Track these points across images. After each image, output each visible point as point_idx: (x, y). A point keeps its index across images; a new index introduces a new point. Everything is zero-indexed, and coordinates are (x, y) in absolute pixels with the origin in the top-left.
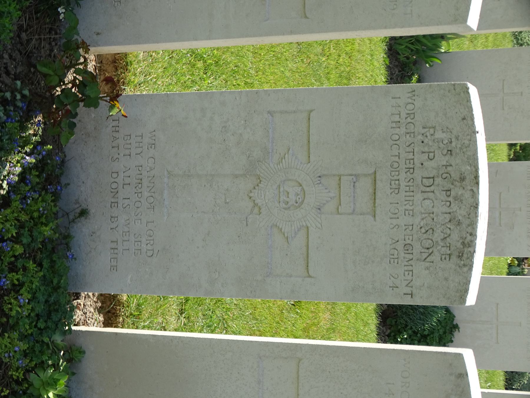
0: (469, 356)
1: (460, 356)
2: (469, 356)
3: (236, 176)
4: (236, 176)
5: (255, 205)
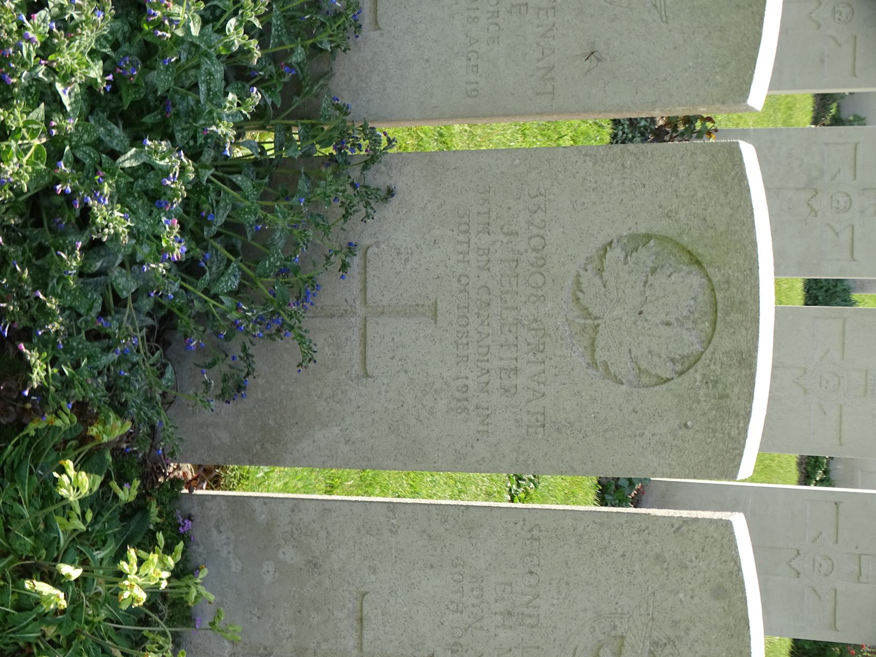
0: (739, 522)
1: (728, 524)
2: (739, 522)
3: (798, 189)
4: (798, 189)
5: (813, 210)
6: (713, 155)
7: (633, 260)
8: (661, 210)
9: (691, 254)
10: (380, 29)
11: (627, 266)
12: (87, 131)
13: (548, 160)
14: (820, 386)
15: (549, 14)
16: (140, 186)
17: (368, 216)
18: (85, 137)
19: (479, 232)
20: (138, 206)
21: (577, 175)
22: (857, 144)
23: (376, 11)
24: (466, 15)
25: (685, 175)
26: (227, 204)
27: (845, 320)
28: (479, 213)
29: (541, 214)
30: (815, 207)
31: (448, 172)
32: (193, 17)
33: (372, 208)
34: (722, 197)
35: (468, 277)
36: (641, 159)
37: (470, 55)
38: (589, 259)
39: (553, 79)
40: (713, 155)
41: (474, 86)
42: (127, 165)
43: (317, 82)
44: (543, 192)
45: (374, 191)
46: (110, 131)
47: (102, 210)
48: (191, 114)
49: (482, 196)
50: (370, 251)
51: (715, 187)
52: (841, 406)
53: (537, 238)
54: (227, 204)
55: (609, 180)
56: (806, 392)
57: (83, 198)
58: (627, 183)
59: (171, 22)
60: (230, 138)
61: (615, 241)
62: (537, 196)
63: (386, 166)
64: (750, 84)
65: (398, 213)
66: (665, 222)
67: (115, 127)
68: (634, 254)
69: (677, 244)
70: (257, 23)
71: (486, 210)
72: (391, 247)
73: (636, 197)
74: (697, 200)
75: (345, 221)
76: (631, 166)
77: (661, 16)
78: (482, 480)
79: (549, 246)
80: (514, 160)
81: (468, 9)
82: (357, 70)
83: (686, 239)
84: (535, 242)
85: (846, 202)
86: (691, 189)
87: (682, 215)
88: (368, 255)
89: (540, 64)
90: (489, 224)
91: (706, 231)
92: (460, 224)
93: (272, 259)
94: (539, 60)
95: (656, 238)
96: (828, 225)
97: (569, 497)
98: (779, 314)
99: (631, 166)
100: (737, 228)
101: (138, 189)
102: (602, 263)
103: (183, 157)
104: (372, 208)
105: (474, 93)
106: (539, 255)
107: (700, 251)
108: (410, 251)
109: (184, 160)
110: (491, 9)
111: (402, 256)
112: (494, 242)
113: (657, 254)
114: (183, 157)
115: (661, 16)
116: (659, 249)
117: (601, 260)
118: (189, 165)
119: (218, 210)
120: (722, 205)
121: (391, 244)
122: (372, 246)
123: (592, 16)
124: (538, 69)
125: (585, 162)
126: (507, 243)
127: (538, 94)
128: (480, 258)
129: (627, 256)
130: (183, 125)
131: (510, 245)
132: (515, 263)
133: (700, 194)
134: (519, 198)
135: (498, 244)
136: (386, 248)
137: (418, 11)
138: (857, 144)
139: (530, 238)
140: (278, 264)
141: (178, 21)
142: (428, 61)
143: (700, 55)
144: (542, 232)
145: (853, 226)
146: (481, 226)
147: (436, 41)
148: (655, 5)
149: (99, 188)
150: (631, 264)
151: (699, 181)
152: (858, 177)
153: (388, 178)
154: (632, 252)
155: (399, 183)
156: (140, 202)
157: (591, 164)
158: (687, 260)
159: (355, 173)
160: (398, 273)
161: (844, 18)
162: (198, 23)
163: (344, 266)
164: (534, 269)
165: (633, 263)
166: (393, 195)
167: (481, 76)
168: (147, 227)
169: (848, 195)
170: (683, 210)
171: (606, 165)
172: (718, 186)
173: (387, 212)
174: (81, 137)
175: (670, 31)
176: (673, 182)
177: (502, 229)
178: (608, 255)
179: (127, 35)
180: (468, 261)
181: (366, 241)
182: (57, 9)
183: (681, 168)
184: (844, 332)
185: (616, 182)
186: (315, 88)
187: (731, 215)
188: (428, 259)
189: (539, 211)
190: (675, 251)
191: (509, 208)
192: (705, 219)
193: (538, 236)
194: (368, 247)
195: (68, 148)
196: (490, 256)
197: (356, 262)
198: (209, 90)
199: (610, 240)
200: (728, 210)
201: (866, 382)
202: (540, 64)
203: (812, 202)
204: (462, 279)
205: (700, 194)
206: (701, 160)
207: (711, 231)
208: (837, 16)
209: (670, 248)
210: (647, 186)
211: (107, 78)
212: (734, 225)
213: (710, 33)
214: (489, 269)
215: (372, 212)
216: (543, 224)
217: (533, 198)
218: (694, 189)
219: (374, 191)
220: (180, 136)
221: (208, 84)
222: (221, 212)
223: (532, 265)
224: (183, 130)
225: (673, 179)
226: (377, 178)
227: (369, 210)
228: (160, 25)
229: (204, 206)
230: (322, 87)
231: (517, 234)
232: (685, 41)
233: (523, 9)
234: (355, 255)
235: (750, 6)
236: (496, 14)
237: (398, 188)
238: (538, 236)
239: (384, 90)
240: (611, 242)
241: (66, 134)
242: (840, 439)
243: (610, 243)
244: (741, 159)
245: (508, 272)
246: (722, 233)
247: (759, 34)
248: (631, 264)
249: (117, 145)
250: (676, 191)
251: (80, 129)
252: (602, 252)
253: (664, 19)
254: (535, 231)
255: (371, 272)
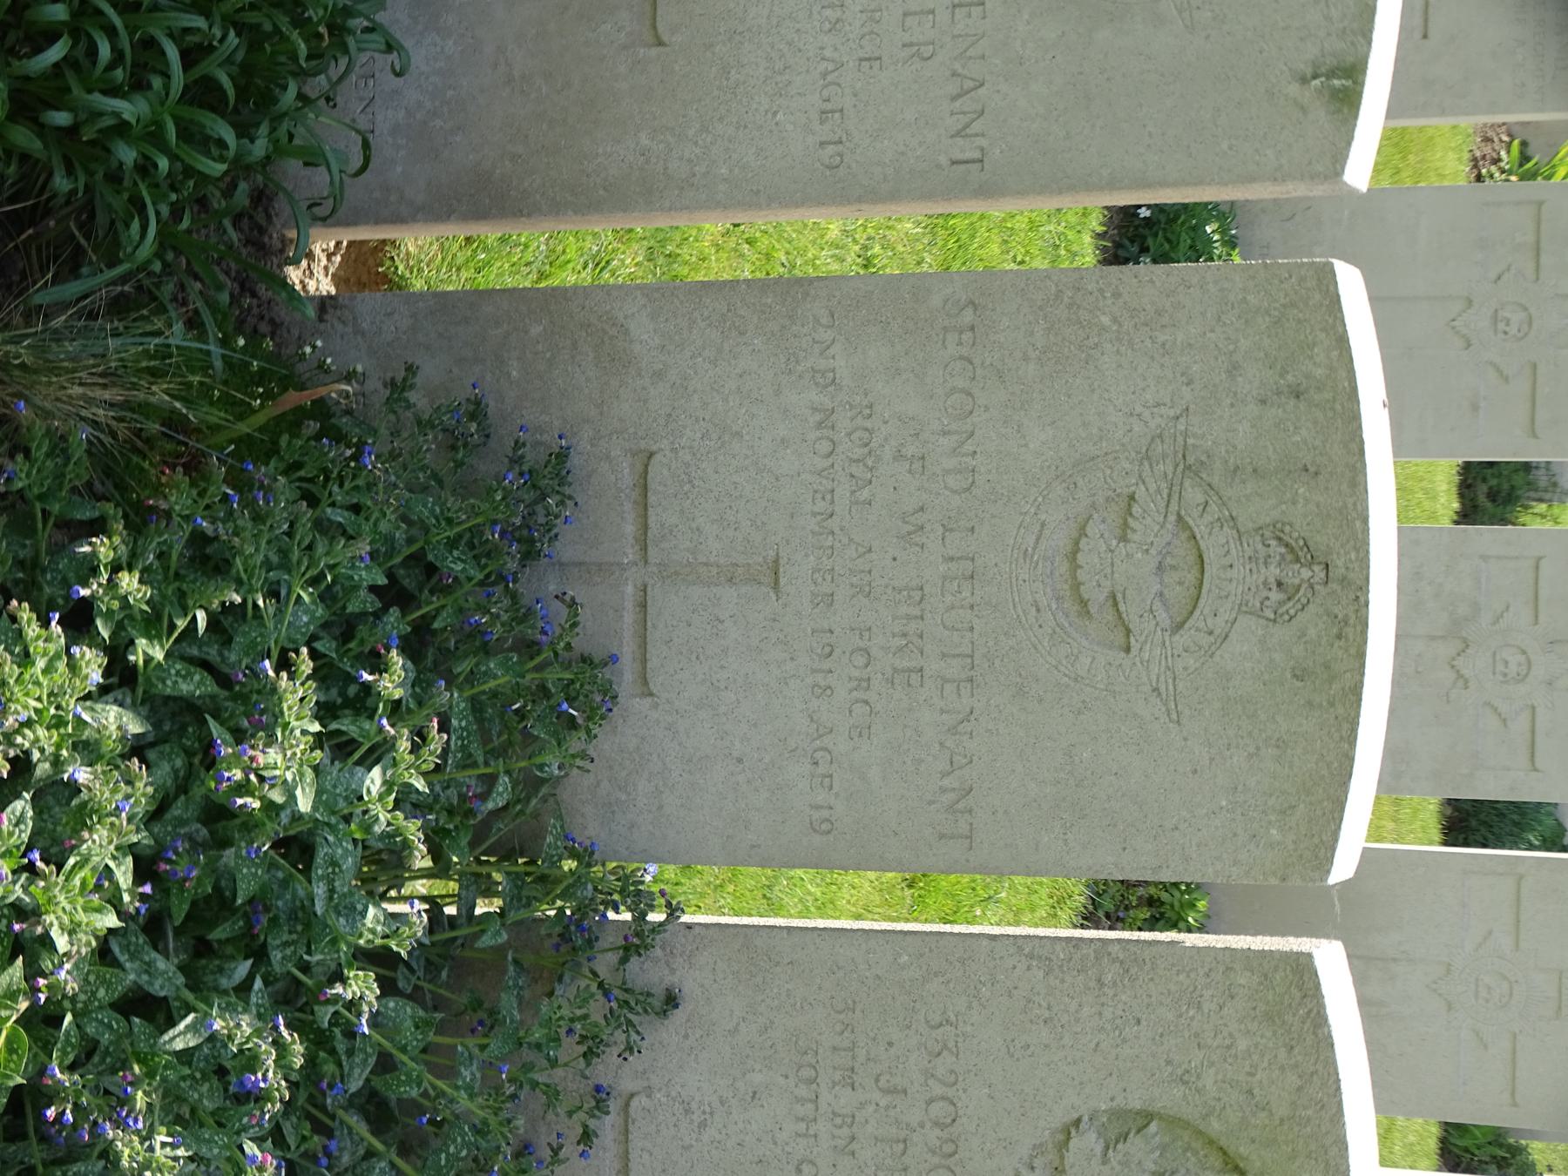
2: (1331, 962)
3: (1433, 638)
4: (1433, 638)
5: (1460, 676)
6: (1266, 976)
7: (1119, 1157)
8: (1170, 1069)
9: (1225, 1153)
10: (651, 694)
11: (1107, 1167)
12: (103, 982)
13: (962, 961)
14: (1477, 996)
15: (963, 691)
16: (206, 1059)
17: (630, 1049)
18: (101, 993)
19: (834, 1084)
20: (201, 1096)
21: (1015, 992)
22: (1539, 559)
23: (644, 661)
24: (809, 680)
25: (1214, 1007)
26: (368, 1055)
27: (1521, 877)
28: (835, 1048)
29: (947, 1058)
30: (1464, 671)
31: (778, 969)
32: (302, 775)
33: (638, 1033)
34: (1282, 1053)
35: (814, 1164)
36: (1133, 971)
37: (819, 755)
38: (1039, 1149)
39: (970, 811)
40: (1266, 976)
41: (825, 813)
42: (179, 1045)
43: (537, 791)
44: (953, 1018)
45: (641, 998)
46: (149, 964)
47: (131, 1141)
48: (300, 914)
49: (842, 1016)
50: (634, 1103)
51: (1269, 1034)
52: (1515, 1036)
53: (941, 1104)
54: (368, 1055)
55: (1073, 1006)
56: (1450, 1007)
57: (95, 1123)
58: (1108, 1013)
59: (262, 779)
60: (370, 1004)
61: (1086, 1118)
62: (941, 1025)
63: (663, 949)
64: (1333, 849)
65: (686, 1036)
66: (1178, 1092)
67: (158, 956)
68: (1120, 1146)
69: (1199, 1133)
70: (420, 784)
71: (846, 1044)
72: (674, 1100)
73: (1124, 1041)
74: (1236, 1056)
75: (588, 1064)
76: (1115, 983)
77: (1168, 711)
78: (866, 881)
79: (964, 1119)
80: (900, 955)
81: (814, 671)
82: (611, 768)
83: (1215, 1127)
84: (938, 1109)
85: (1520, 665)
86: (1225, 1034)
87: (1208, 1080)
88: (632, 1110)
89: (946, 782)
90: (853, 1069)
91: (1254, 1114)
92: (800, 1067)
93: (452, 1149)
94: (944, 775)
95: (1161, 1118)
96: (1488, 704)
97: (1029, 914)
98: (1408, 541)
99: (1115, 983)
100: (1309, 1112)
101: (201, 1065)
102: (1062, 1158)
103: (282, 1028)
104: (638, 1033)
105: (825, 827)
106: (945, 1135)
107: (1242, 1149)
108: (708, 1109)
109: (285, 1033)
110: (856, 673)
111: (695, 1117)
112: (862, 1105)
113: (1164, 1148)
114: (282, 1028)
115: (1168, 711)
116: (1167, 1139)
117: (1060, 1150)
118: (294, 1042)
119: (351, 1068)
120: (1282, 1068)
121: (674, 1094)
122: (638, 1093)
123: (1040, 701)
124: (943, 790)
125: (1029, 968)
126: (887, 1108)
127: (942, 836)
128: (837, 1132)
129: (1107, 1148)
130: (285, 937)
131: (892, 1113)
132: (901, 1146)
133: (1242, 1044)
134: (909, 1027)
135: (871, 1108)
136: (664, 1100)
137: (722, 667)
138: (1539, 559)
139: (929, 1102)
140: (464, 1153)
141: (275, 777)
142: (740, 761)
143: (1240, 788)
144: (950, 1093)
145: (1533, 708)
146: (839, 1073)
147: (755, 725)
148: (1156, 690)
149: (126, 1101)
150: (1114, 1163)
151: (1240, 1021)
152: (1541, 618)
153: (666, 972)
154: (1117, 1142)
155: (690, 980)
156: (206, 1086)
157: (1041, 973)
158: (1218, 1164)
159: (605, 964)
160: (688, 1148)
161: (1513, 330)
162: (311, 785)
163: (587, 1137)
164: (936, 1160)
165: (1119, 1163)
166: (676, 1006)
167: (837, 795)
168: (216, 1151)
169: (1524, 652)
170: (1212, 1071)
171: (1068, 979)
172: (1275, 1033)
173: (665, 1036)
174: (94, 993)
175: (1185, 739)
176: (1192, 1018)
177: (877, 1080)
178: (1072, 1144)
179: (182, 773)
180: (816, 1136)
181: (627, 1084)
182: (47, 765)
183: (1207, 994)
184: (1518, 899)
185: (1086, 1011)
186: (534, 802)
187: (1300, 1089)
188: (741, 1125)
189: (945, 1053)
190: (1197, 1145)
191: (890, 1044)
192: (1250, 1092)
193: (943, 1098)
194: (632, 1095)
195: (69, 1018)
196: (855, 1129)
197: (607, 1127)
198: (332, 891)
199: (1076, 1116)
200: (1292, 1079)
201: (1560, 992)
202: (946, 782)
203: (1459, 662)
204: (804, 1167)
205: (1242, 1044)
206: (1242, 981)
207: (1263, 1115)
208: (1501, 326)
209: (1186, 1139)
210: (1144, 1023)
211: (141, 890)
212: (1305, 1108)
213: (1258, 748)
214: (853, 1154)
215: (638, 1038)
216: (952, 1079)
217: (933, 1027)
218: (1231, 1035)
219: (641, 998)
220: (279, 956)
221: (331, 882)
222: (357, 1071)
223: (934, 1153)
224: (286, 944)
225: (1191, 1013)
226: (648, 973)
227: (634, 1036)
228: (243, 788)
229: (325, 1068)
230: (545, 800)
231: (905, 1092)
232: (1212, 759)
233: (915, 678)
234: (608, 1113)
235: (1332, 704)
236: (865, 684)
237: (685, 990)
238: (943, 1098)
239: (661, 807)
240: (1079, 1120)
241: (64, 996)
242: (1513, 1094)
243: (1077, 1122)
244: (1318, 986)
245: (888, 1161)
246: (1282, 1120)
247: (1350, 759)
248: (1114, 1163)
249: (162, 988)
250: (1197, 1035)
251: (92, 978)
252: (1062, 1137)
253: (1174, 716)
254: (938, 1090)
255: (636, 1141)
